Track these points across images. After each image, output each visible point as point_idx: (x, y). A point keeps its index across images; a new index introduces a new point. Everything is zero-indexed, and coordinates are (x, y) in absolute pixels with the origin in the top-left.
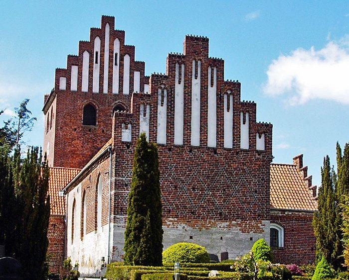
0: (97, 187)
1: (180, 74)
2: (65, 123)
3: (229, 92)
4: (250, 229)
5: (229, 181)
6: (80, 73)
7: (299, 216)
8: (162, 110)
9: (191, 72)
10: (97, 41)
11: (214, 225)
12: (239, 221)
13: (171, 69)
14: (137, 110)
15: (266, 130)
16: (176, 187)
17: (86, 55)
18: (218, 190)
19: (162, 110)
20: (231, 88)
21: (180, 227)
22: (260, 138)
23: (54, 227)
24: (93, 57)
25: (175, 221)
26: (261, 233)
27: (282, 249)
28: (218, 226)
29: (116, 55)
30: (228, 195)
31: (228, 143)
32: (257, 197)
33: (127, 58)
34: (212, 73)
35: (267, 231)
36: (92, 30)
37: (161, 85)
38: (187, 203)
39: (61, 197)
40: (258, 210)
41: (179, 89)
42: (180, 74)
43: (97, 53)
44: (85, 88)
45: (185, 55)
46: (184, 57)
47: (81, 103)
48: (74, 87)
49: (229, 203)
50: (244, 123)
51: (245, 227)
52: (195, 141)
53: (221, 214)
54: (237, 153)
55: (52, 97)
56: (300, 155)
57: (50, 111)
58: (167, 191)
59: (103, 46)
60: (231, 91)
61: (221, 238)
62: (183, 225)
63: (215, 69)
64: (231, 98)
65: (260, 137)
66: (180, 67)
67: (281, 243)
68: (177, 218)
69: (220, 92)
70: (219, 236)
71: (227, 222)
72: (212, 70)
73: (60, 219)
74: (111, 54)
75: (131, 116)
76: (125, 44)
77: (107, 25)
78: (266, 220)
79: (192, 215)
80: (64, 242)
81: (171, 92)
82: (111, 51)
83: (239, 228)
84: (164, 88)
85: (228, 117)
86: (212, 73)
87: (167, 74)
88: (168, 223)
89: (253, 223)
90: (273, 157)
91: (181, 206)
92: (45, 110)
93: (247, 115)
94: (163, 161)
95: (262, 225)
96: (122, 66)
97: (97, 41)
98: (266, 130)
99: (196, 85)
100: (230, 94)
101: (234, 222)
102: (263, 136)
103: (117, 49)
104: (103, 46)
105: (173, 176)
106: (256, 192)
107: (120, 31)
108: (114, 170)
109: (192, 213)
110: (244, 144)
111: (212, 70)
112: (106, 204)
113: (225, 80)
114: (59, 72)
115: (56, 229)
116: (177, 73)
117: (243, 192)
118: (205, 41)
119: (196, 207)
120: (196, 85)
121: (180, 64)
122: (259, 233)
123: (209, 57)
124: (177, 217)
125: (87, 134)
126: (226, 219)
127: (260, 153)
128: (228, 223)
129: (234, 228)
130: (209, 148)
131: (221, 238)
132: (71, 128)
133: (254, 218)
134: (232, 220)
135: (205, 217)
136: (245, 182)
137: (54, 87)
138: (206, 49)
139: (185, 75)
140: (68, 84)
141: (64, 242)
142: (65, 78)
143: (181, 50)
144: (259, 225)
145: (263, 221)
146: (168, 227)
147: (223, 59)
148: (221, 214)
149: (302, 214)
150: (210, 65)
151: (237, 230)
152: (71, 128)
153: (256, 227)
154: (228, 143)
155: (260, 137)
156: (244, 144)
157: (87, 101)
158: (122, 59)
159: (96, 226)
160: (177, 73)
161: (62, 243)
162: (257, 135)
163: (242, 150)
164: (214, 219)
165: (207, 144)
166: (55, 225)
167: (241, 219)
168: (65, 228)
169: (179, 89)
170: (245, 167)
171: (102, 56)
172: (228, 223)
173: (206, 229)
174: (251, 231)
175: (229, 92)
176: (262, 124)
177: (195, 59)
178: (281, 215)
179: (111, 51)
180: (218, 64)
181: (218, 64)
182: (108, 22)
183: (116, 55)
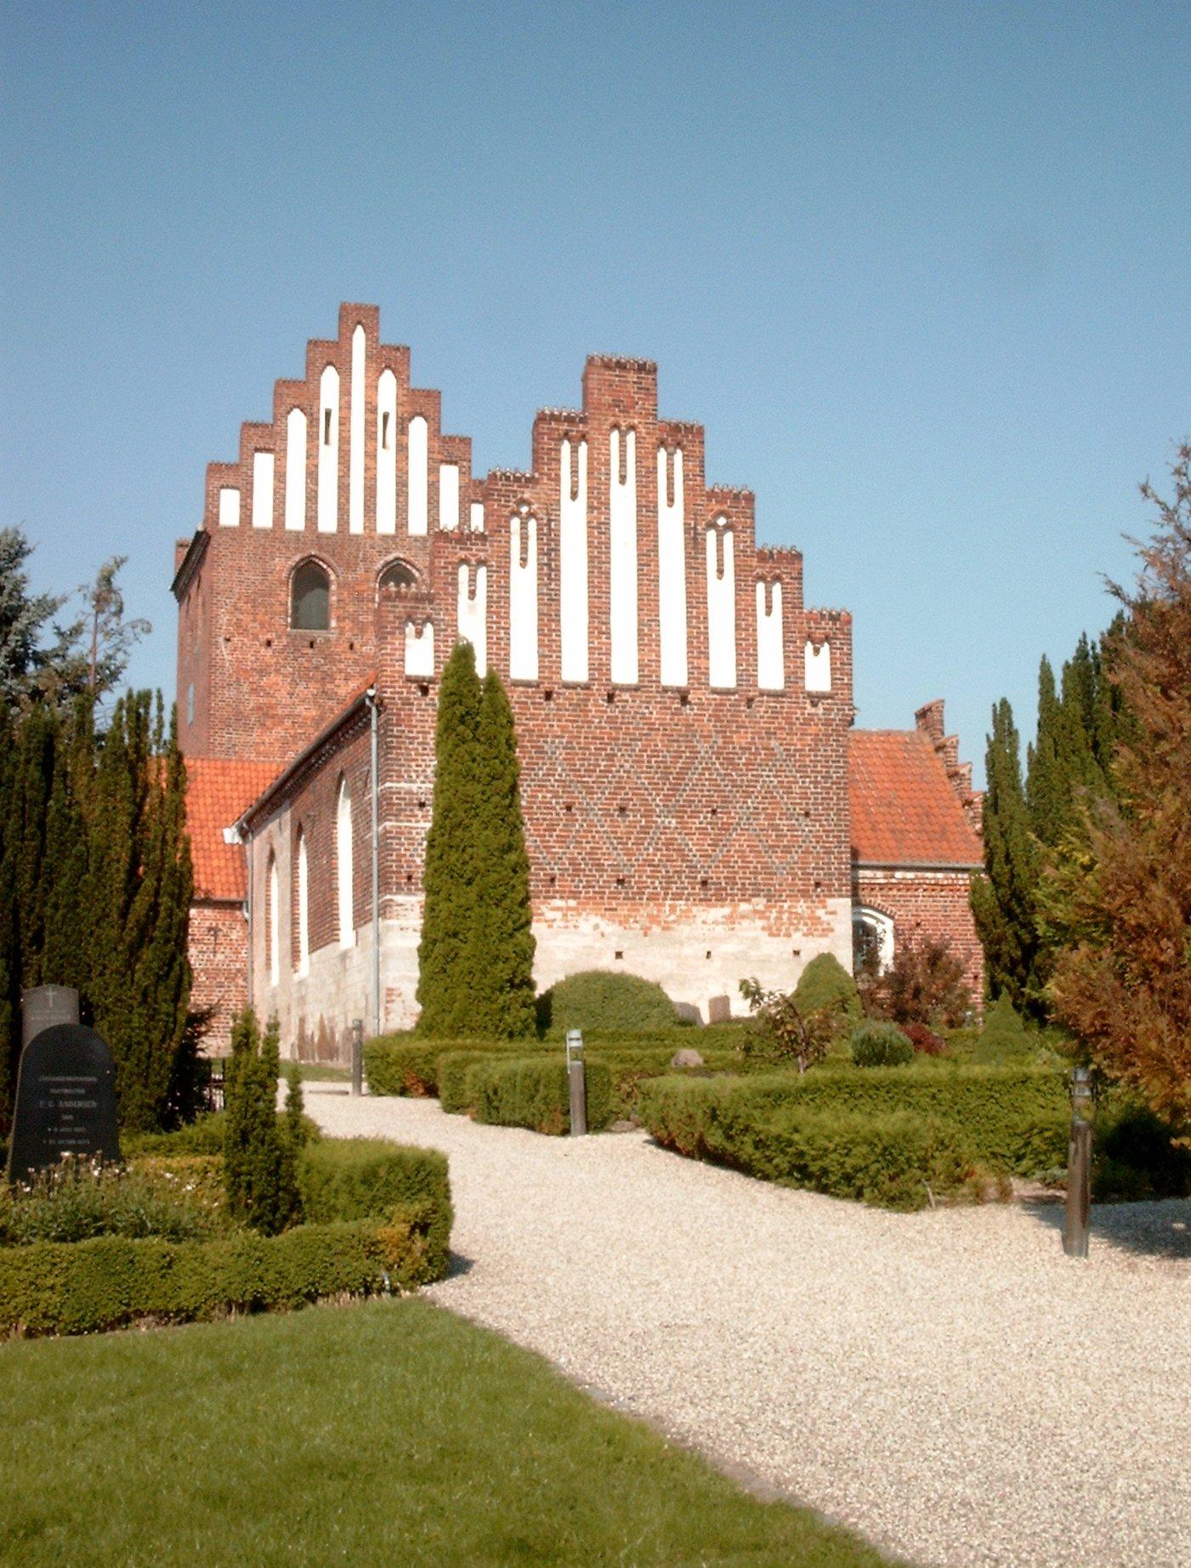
1: (574, 472)
2: (238, 624)
6: (280, 476)
8: (524, 583)
11: (687, 915)
12: (760, 903)
15: (833, 630)
16: (569, 808)
19: (524, 583)
30: (726, 828)
31: (723, 673)
34: (670, 466)
42: (574, 472)
47: (283, 564)
51: (779, 918)
53: (704, 883)
59: (345, 391)
62: (595, 919)
65: (817, 651)
79: (620, 891)
81: (549, 525)
83: (760, 923)
86: (670, 466)
89: (802, 906)
96: (402, 449)
99: (623, 501)
104: (345, 391)
106: (807, 814)
110: (771, 676)
117: (771, 817)
120: (623, 501)
124: (575, 895)
125: (303, 655)
129: (745, 923)
133: (805, 894)
141: (245, 980)
144: (820, 913)
145: (830, 901)
154: (723, 673)
155: (817, 651)
156: (771, 676)
158: (402, 430)
161: (241, 982)
162: (809, 647)
170: (773, 743)
171: (345, 422)
172: (727, 911)
174: (797, 930)
179: (371, 408)
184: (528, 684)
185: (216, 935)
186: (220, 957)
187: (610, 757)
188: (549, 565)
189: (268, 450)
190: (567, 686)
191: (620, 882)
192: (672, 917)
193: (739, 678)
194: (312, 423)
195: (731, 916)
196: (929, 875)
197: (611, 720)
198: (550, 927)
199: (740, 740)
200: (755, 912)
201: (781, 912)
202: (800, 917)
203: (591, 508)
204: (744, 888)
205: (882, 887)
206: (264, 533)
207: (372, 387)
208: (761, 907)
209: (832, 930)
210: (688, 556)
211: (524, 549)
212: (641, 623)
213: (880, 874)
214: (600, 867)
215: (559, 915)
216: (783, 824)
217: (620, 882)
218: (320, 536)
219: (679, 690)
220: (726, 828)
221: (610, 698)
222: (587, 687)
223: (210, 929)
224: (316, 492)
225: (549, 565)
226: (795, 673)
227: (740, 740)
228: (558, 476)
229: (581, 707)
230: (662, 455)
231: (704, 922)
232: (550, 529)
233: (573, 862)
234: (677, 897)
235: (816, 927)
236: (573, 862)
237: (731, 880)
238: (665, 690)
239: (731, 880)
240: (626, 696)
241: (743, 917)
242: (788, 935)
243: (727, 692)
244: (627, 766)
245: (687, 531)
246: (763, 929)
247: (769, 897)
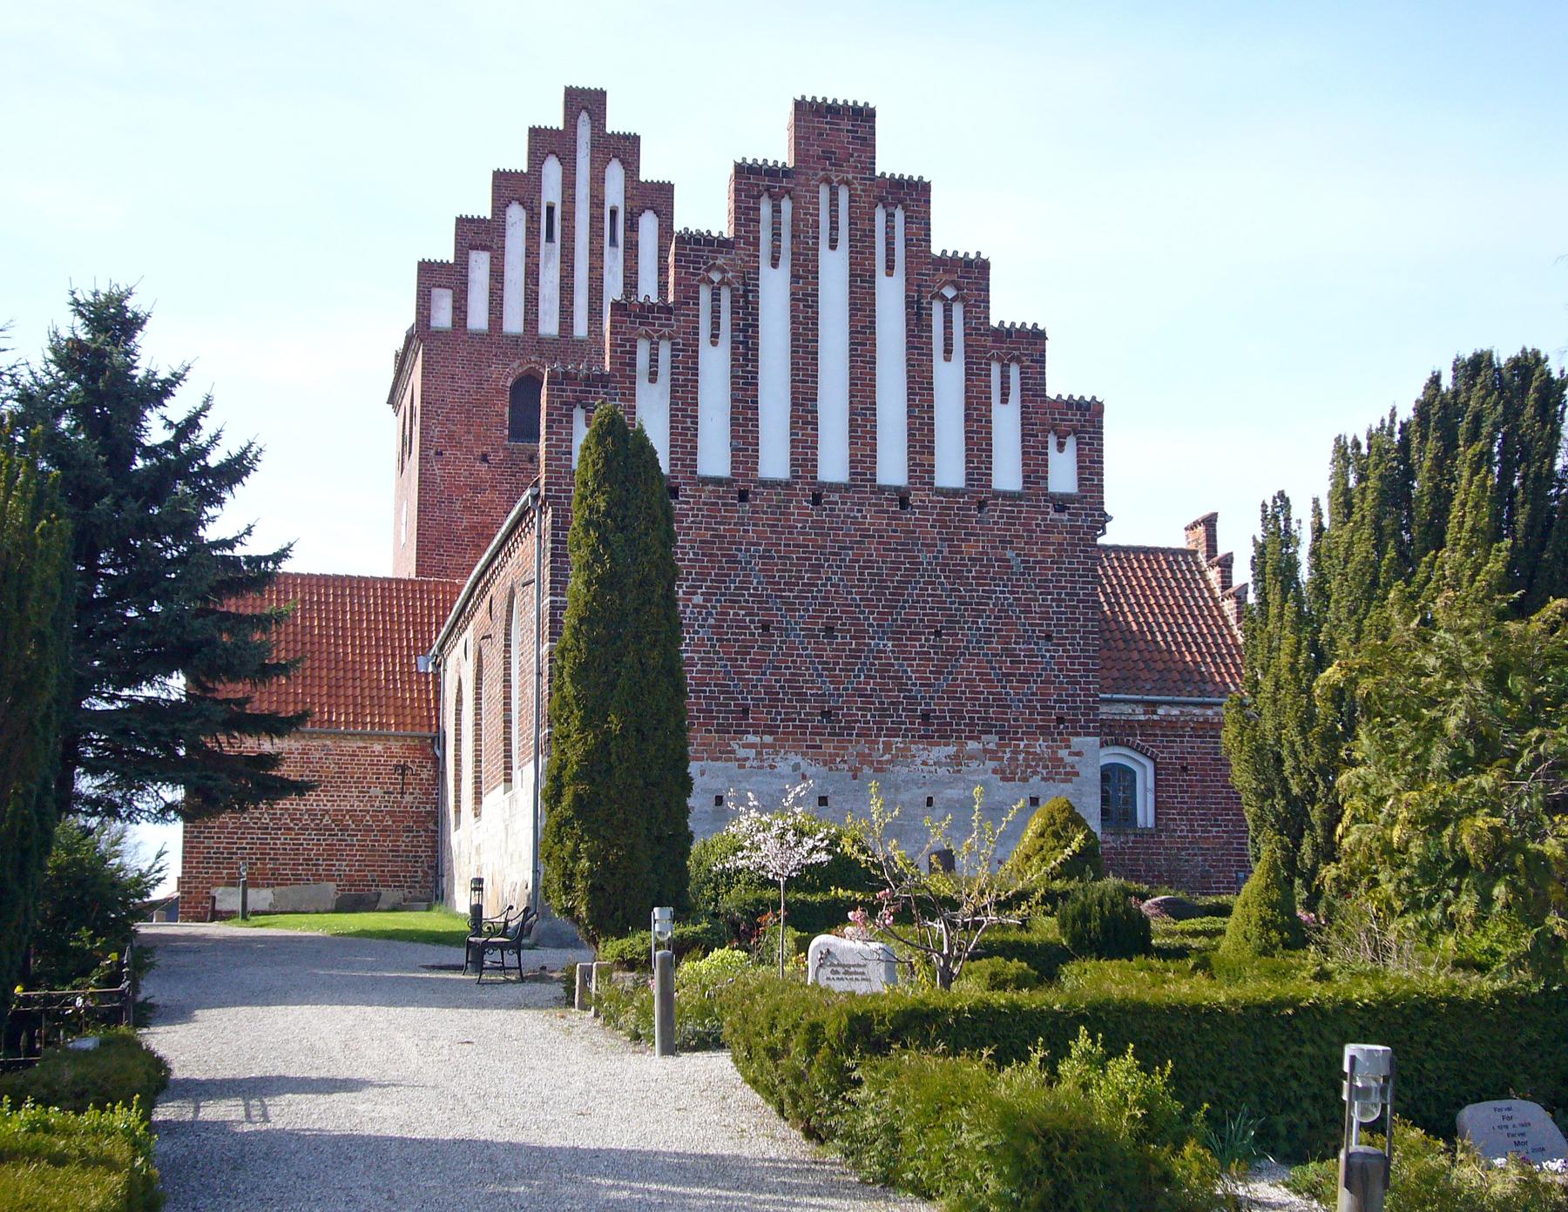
0: (507, 635)
1: (776, 235)
2: (451, 437)
3: (949, 292)
4: (1028, 766)
5: (953, 603)
6: (497, 275)
7: (1206, 721)
8: (715, 364)
9: (816, 225)
10: (552, 170)
11: (904, 756)
12: (992, 741)
13: (744, 213)
14: (626, 361)
15: (1084, 421)
16: (765, 627)
17: (516, 216)
18: (915, 636)
19: (715, 364)
20: (955, 277)
21: (783, 767)
22: (889, 274)
23: (403, 774)
24: (539, 222)
25: (764, 745)
26: (1070, 781)
27: (1143, 833)
28: (919, 761)
29: (613, 213)
30: (951, 652)
31: (950, 471)
32: (1052, 657)
33: (648, 224)
34: (890, 228)
35: (1090, 773)
36: (535, 133)
37: (708, 270)
38: (807, 682)
39: (427, 674)
40: (1056, 701)
41: (774, 288)
42: (776, 235)
43: (550, 209)
44: (514, 323)
45: (791, 165)
46: (786, 172)
47: (505, 374)
48: (478, 319)
49: (954, 679)
50: (1004, 401)
51: (1013, 759)
52: (833, 465)
53: (925, 717)
54: (981, 505)
55: (410, 355)
56: (1206, 512)
57: (406, 401)
58: (736, 640)
59: (569, 184)
60: (958, 288)
61: (930, 802)
62: (795, 759)
63: (899, 215)
64: (958, 311)
65: (1061, 447)
66: (777, 210)
67: (1145, 814)
68: (771, 733)
69: (919, 291)
70: (921, 794)
71: (947, 745)
72: (890, 216)
73: (423, 749)
74: (597, 212)
75: (603, 380)
76: (642, 179)
77: (584, 116)
78: (1088, 734)
79: (822, 725)
80: (436, 823)
81: (745, 296)
82: (597, 201)
83: (991, 765)
84: (722, 282)
85: (949, 378)
86: (890, 228)
87: (728, 233)
88: (741, 753)
89: (1040, 746)
90: (1106, 518)
91: (785, 694)
92: (393, 399)
93: (1014, 371)
94: (773, 545)
95: (1070, 754)
96: (632, 249)
97: (552, 170)
98: (1084, 421)
99: (834, 269)
100: (954, 299)
101: (972, 745)
102: (1071, 442)
103: (615, 194)
104: (569, 184)
105: (756, 589)
106: (1048, 638)
107: (626, 137)
108: (547, 572)
109: (823, 714)
110: (1007, 474)
111: (890, 216)
112: (529, 691)
113: (994, 322)
114: (430, 273)
115: (409, 778)
116: (765, 236)
117: (1005, 640)
118: (863, 117)
119: (840, 696)
120: (834, 269)
121: (776, 200)
122: (1064, 781)
123: (878, 173)
124: (771, 730)
125: (522, 470)
126: (945, 737)
127: (1062, 503)
128: (952, 750)
129: (974, 765)
130: (882, 489)
131: (930, 802)
132: (472, 453)
133: (1044, 731)
134: (968, 738)
135: (870, 729)
136: (1010, 605)
137: (413, 320)
138: (867, 142)
139: (794, 236)
140: (460, 310)
141: (436, 823)
142: (450, 292)
143: (777, 149)
144: (1063, 753)
145: (1074, 740)
146: (741, 767)
147: (1040, 327)
148: (925, 717)
149: (1216, 714)
150: (881, 199)
151: (985, 772)
152: (472, 453)
153: (1050, 759)
154: (950, 471)
155: (1061, 447)
156: (1007, 474)
157: (521, 365)
158: (632, 227)
159: (508, 767)
160: (765, 236)
161: (431, 826)
162: (1052, 441)
163: (998, 494)
164: (905, 736)
165: (874, 474)
166: (404, 768)
167: (997, 733)
168: (440, 774)
169: (774, 288)
170: (1009, 554)
171: (569, 216)
172: (952, 750)
173: (876, 770)
174: (1035, 773)
175: (949, 292)
176: (829, 107)
177: (828, 181)
178: (1142, 718)
179: (597, 201)
180: (912, 196)
181: (912, 196)
182: (585, 108)
183: (613, 213)
184: (718, 481)
185: (403, 774)
186: (408, 798)
187: (816, 568)
188: (745, 343)
189: (484, 248)
190: (765, 484)
191: (826, 714)
192: (887, 757)
193: (969, 477)
194: (533, 218)
195: (956, 756)
196: (1197, 711)
197: (818, 525)
198: (742, 767)
199: (969, 549)
200: (985, 751)
201: (1016, 752)
202: (1038, 758)
203: (795, 277)
204: (972, 724)
205: (1142, 724)
206: (478, 335)
207: (598, 180)
208: (992, 746)
209: (1077, 774)
210: (910, 334)
211: (716, 325)
212: (853, 412)
213: (1139, 710)
214: (802, 698)
215: (752, 753)
216: (1020, 648)
217: (826, 714)
218: (541, 341)
219: (897, 489)
220: (951, 652)
221: (816, 500)
222: (787, 485)
223: (396, 766)
224: (537, 293)
225: (745, 343)
226: (1035, 468)
227: (969, 549)
228: (757, 239)
229: (782, 509)
230: (880, 216)
231: (924, 763)
232: (747, 302)
233: (769, 691)
234: (893, 733)
235: (1058, 771)
236: (769, 691)
237: (957, 714)
238: (882, 489)
239: (957, 714)
240: (835, 497)
241: (971, 758)
242: (1025, 780)
243: (954, 493)
244: (835, 579)
245: (908, 305)
246: (995, 771)
247: (1002, 734)
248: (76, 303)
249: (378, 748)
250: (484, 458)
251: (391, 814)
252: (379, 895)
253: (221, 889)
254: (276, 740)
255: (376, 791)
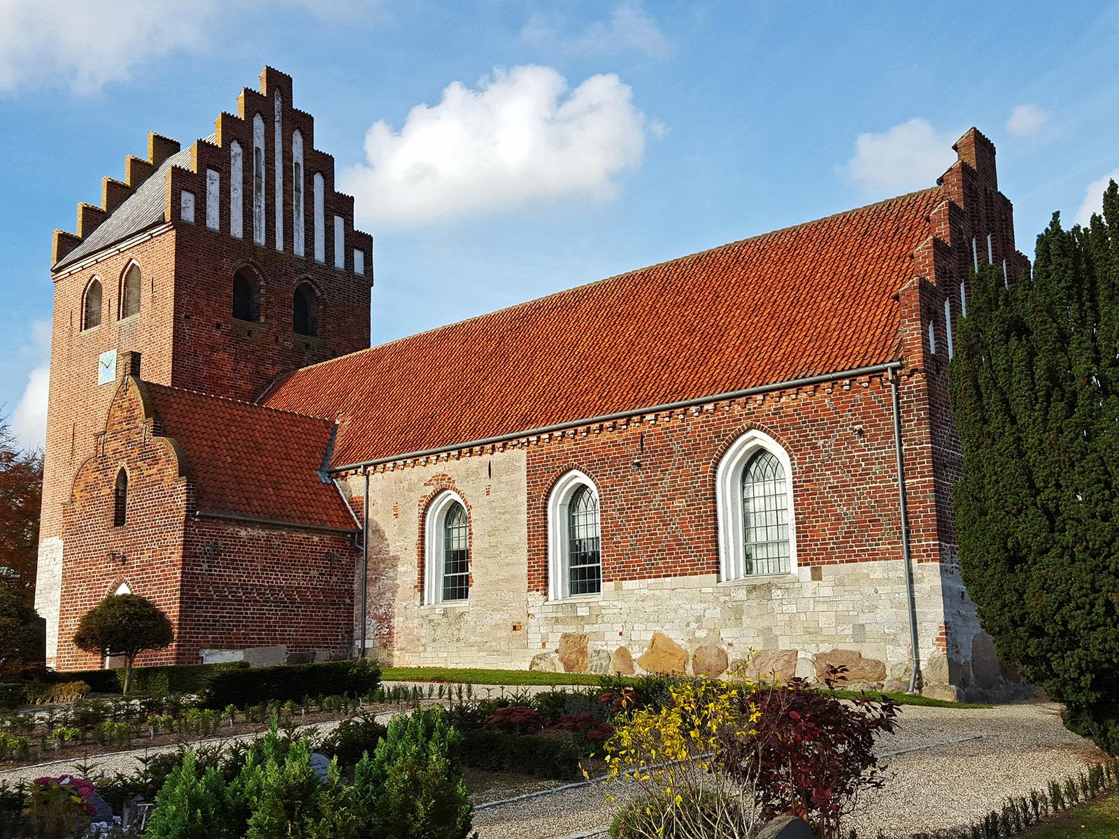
2: (196, 306)
47: (229, 266)
74: (288, 163)
96: (309, 196)
157: (242, 263)
161: (348, 601)
186: (334, 579)
207: (288, 142)
248: (546, 120)
249: (316, 539)
250: (218, 326)
251: (323, 591)
252: (315, 653)
253: (207, 651)
254: (249, 530)
255: (314, 573)
